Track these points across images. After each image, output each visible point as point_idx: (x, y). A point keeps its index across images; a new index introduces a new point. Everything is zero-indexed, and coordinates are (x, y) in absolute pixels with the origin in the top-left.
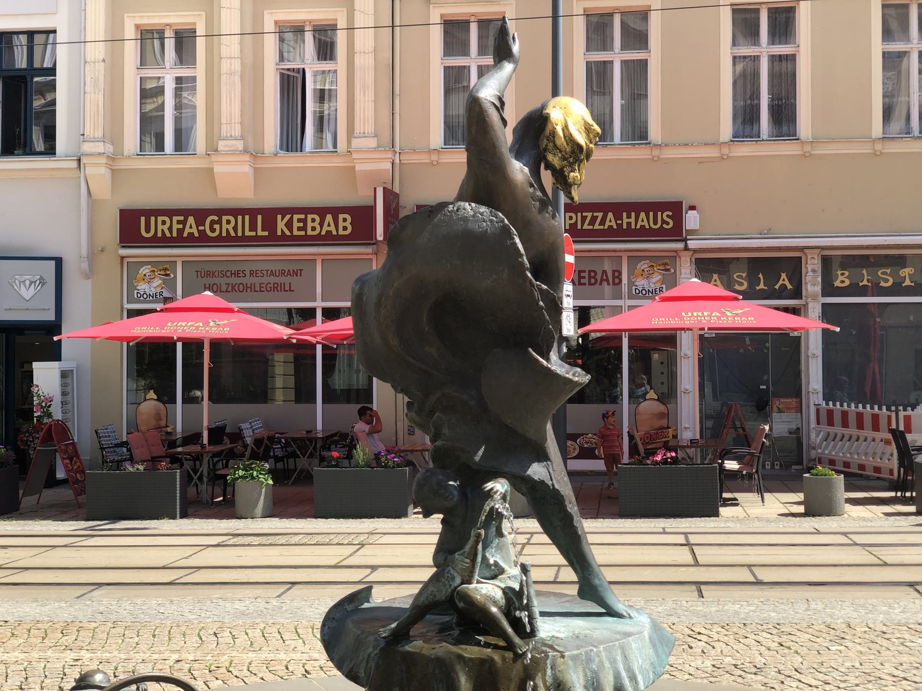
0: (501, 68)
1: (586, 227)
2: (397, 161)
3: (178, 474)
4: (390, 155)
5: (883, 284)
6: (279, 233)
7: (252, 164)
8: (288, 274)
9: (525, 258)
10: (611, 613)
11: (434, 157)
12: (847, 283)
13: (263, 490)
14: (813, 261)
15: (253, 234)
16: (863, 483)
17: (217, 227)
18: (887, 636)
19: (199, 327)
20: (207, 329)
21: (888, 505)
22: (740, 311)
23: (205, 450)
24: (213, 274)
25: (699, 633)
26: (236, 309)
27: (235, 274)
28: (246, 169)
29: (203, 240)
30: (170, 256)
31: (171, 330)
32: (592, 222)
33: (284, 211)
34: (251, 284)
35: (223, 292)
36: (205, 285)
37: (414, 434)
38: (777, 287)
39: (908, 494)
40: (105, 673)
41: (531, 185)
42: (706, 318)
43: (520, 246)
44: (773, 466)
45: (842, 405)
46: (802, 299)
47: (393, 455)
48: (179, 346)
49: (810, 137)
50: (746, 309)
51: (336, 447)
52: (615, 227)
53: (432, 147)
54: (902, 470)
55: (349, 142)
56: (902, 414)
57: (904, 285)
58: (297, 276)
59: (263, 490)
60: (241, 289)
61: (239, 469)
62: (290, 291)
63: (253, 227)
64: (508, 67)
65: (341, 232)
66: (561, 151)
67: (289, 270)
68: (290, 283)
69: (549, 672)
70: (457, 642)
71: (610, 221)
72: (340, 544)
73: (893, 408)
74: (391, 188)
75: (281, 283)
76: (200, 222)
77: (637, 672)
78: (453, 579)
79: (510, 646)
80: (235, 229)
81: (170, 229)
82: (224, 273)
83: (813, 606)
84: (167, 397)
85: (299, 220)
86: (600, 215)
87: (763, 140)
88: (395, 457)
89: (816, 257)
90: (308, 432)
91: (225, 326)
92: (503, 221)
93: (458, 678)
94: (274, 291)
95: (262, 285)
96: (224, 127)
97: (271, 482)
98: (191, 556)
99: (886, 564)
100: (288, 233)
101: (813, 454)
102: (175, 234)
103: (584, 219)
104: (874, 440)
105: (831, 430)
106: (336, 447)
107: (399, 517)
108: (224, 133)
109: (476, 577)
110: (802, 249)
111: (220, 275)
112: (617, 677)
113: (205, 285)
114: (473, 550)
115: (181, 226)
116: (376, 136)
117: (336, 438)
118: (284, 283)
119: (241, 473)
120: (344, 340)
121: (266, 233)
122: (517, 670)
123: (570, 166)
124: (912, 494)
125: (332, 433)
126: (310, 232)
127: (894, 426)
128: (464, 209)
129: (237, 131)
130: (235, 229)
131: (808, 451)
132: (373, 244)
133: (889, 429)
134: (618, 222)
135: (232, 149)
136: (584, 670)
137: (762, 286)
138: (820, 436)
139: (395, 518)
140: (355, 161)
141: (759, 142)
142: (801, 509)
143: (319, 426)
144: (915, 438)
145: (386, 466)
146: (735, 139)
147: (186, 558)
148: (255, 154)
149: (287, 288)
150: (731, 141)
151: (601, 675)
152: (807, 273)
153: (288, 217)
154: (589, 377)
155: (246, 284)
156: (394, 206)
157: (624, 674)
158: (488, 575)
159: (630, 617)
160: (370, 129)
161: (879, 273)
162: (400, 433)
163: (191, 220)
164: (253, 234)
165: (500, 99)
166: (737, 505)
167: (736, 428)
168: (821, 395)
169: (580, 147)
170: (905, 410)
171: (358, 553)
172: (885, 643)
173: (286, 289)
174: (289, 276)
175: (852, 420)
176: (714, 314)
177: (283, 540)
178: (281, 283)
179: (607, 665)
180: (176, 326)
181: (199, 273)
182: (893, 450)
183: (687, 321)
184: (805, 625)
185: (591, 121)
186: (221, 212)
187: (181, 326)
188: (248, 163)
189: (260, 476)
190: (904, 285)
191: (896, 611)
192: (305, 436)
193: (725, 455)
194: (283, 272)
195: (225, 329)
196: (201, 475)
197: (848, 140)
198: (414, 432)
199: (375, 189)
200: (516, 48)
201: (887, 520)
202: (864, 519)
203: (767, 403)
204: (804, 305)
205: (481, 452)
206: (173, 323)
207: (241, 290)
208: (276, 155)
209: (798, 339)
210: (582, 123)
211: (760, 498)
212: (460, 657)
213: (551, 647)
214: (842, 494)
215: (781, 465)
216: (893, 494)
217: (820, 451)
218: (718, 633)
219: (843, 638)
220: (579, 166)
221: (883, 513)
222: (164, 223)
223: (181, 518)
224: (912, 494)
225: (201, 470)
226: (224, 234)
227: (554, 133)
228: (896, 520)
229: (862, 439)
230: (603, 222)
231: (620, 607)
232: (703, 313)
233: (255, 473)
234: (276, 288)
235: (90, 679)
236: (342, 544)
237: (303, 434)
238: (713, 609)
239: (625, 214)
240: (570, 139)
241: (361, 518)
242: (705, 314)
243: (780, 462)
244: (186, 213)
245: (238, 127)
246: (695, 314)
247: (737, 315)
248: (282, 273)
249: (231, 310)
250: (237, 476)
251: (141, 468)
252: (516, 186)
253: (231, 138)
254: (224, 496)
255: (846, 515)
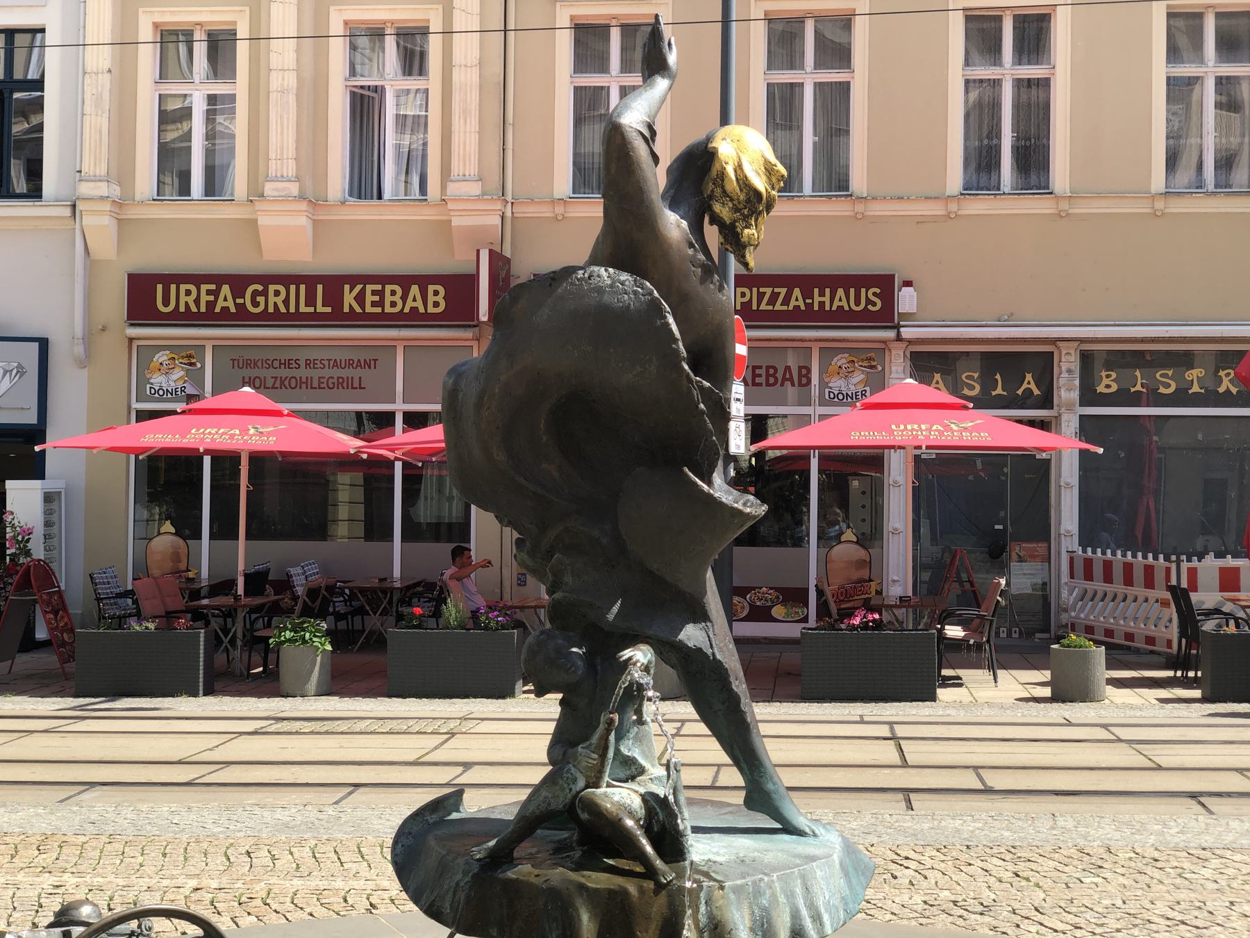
0: (651, 85)
1: (763, 307)
2: (509, 214)
3: (202, 635)
4: (499, 206)
5: (1162, 390)
6: (346, 309)
7: (310, 216)
8: (357, 365)
9: (680, 344)
10: (789, 829)
11: (559, 209)
12: (1114, 387)
13: (319, 659)
14: (1068, 357)
15: (311, 310)
16: (1132, 658)
17: (261, 299)
18: (1159, 865)
19: (235, 435)
20: (245, 438)
21: (1164, 688)
22: (970, 424)
23: (239, 603)
24: (255, 364)
25: (907, 858)
26: (286, 412)
27: (285, 364)
28: (303, 221)
29: (241, 317)
30: (197, 339)
31: (196, 439)
32: (774, 297)
33: (353, 280)
34: (307, 378)
35: (315, 388)
36: (244, 377)
37: (525, 585)
38: (1020, 392)
39: (1191, 674)
40: (95, 905)
41: (691, 245)
42: (924, 433)
43: (674, 327)
44: (1009, 635)
45: (1104, 553)
46: (1052, 408)
47: (496, 613)
48: (207, 460)
49: (1068, 191)
50: (978, 422)
51: (419, 601)
52: (803, 308)
53: (557, 195)
54: (1184, 641)
55: (443, 188)
56: (1185, 566)
57: (1190, 392)
58: (370, 368)
59: (319, 659)
60: (293, 385)
61: (285, 629)
62: (360, 388)
63: (311, 301)
64: (661, 84)
65: (431, 310)
66: (732, 200)
67: (359, 360)
68: (360, 378)
69: (703, 908)
70: (578, 867)
71: (797, 300)
72: (421, 733)
73: (1174, 558)
74: (499, 251)
75: (348, 378)
76: (238, 292)
77: (823, 910)
78: (575, 780)
79: (650, 873)
80: (286, 302)
81: (197, 302)
82: (270, 363)
83: (1061, 822)
84: (188, 530)
85: (374, 293)
86: (783, 291)
87: (1004, 193)
88: (498, 616)
89: (1072, 352)
90: (382, 580)
91: (269, 434)
92: (651, 294)
93: (579, 915)
94: (338, 388)
95: (322, 380)
96: (272, 164)
97: (329, 647)
98: (217, 746)
99: (1159, 768)
100: (358, 310)
101: (1064, 618)
102: (203, 309)
103: (761, 296)
104: (1146, 600)
105: (1089, 586)
106: (419, 601)
107: (503, 697)
108: (272, 172)
109: (606, 778)
110: (1054, 341)
111: (265, 365)
112: (795, 915)
113: (244, 377)
114: (603, 742)
115: (212, 298)
116: (481, 180)
117: (420, 589)
118: (352, 378)
119: (288, 634)
120: (432, 455)
121: (329, 310)
122: (659, 905)
123: (744, 220)
124: (1196, 674)
125: (415, 581)
126: (388, 309)
127: (1174, 582)
128: (599, 276)
129: (290, 169)
130: (286, 302)
131: (1058, 613)
132: (475, 326)
133: (1167, 586)
134: (808, 301)
135: (283, 194)
136: (751, 907)
137: (999, 391)
138: (1074, 594)
139: (498, 698)
140: (452, 213)
141: (998, 197)
142: (1046, 692)
143: (397, 573)
144: (1202, 598)
145: (486, 628)
146: (966, 192)
147: (210, 750)
148: (314, 201)
149: (356, 384)
150: (962, 194)
151: (774, 914)
152: (1060, 374)
153: (359, 287)
154: (765, 508)
155: (301, 378)
156: (503, 274)
157: (804, 912)
158: (622, 776)
159: (815, 835)
160: (472, 169)
161: (1158, 375)
162: (507, 584)
163: (226, 289)
164: (311, 310)
165: (650, 127)
166: (960, 685)
167: (960, 582)
168: (1076, 539)
169: (758, 194)
170: (1189, 560)
171: (446, 745)
172: (1157, 874)
173: (314, 386)
174: (336, 368)
175: (1118, 572)
176: (934, 428)
177: (343, 727)
178: (348, 378)
179: (782, 899)
180: (203, 433)
181: (236, 362)
182: (1171, 614)
183: (898, 436)
184: (1049, 848)
185: (773, 160)
186: (266, 280)
187: (210, 433)
188: (306, 213)
189: (315, 639)
190: (1190, 392)
191: (1172, 832)
192: (377, 585)
193: (945, 618)
194: (351, 362)
195: (270, 439)
196: (234, 637)
197: (1119, 195)
198: (525, 582)
199: (478, 251)
200: (672, 58)
201: (1163, 708)
202: (1132, 707)
203: (1003, 550)
204: (1056, 417)
205: (615, 609)
206: (198, 430)
207: (293, 385)
208: (343, 203)
209: (1047, 462)
210: (762, 162)
211: (992, 677)
212: (582, 887)
213: (706, 875)
214: (1103, 673)
215: (1021, 633)
216: (1170, 673)
217: (1073, 614)
218: (931, 858)
219: (1101, 867)
220: (756, 220)
221: (1157, 699)
222: (188, 293)
223: (205, 694)
224: (1196, 674)
225: (233, 630)
226: (271, 310)
227: (722, 175)
228: (1174, 708)
229: (1130, 599)
230: (786, 301)
231: (801, 822)
232: (919, 427)
233: (307, 635)
234: (341, 383)
235: (74, 912)
236: (425, 733)
237: (375, 583)
238: (926, 826)
239: (816, 291)
240: (744, 183)
241: (451, 697)
242: (923, 427)
243: (1020, 629)
244: (219, 280)
245: (292, 164)
246: (909, 427)
247: (965, 429)
248: (349, 364)
249: (278, 413)
250: (283, 638)
251: (151, 626)
252: (670, 246)
253: (282, 179)
254: (265, 666)
255: (1107, 701)
